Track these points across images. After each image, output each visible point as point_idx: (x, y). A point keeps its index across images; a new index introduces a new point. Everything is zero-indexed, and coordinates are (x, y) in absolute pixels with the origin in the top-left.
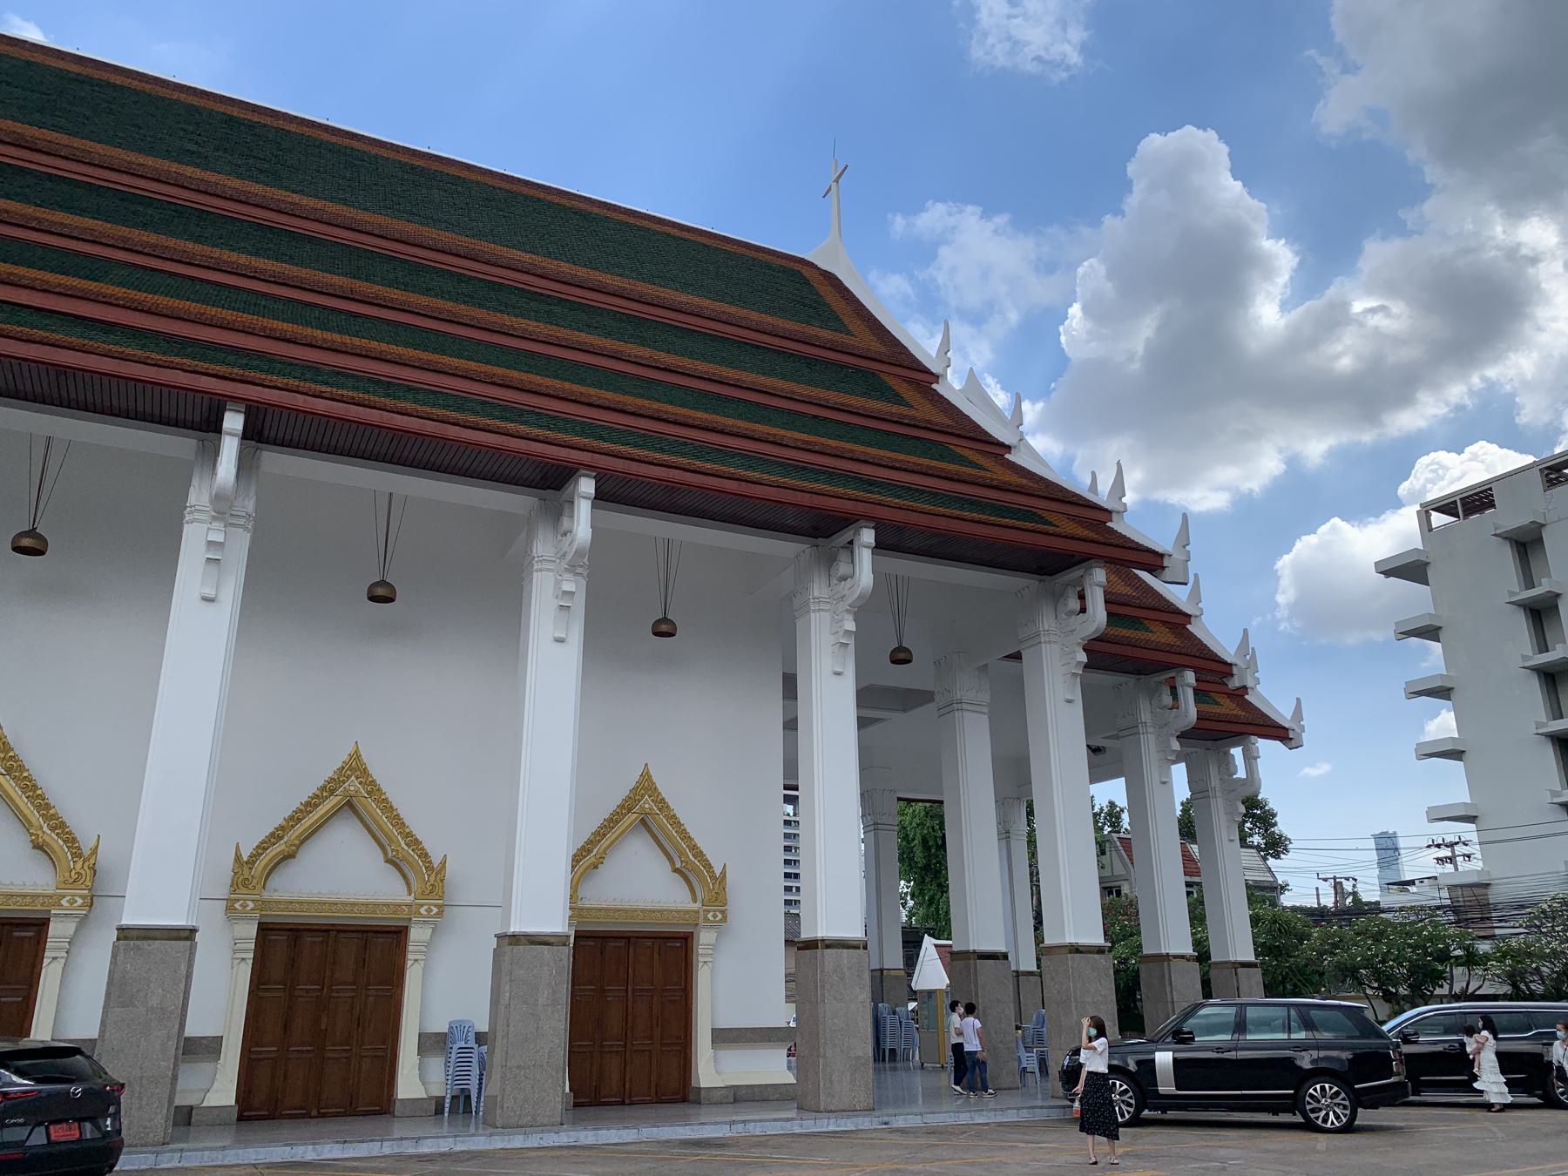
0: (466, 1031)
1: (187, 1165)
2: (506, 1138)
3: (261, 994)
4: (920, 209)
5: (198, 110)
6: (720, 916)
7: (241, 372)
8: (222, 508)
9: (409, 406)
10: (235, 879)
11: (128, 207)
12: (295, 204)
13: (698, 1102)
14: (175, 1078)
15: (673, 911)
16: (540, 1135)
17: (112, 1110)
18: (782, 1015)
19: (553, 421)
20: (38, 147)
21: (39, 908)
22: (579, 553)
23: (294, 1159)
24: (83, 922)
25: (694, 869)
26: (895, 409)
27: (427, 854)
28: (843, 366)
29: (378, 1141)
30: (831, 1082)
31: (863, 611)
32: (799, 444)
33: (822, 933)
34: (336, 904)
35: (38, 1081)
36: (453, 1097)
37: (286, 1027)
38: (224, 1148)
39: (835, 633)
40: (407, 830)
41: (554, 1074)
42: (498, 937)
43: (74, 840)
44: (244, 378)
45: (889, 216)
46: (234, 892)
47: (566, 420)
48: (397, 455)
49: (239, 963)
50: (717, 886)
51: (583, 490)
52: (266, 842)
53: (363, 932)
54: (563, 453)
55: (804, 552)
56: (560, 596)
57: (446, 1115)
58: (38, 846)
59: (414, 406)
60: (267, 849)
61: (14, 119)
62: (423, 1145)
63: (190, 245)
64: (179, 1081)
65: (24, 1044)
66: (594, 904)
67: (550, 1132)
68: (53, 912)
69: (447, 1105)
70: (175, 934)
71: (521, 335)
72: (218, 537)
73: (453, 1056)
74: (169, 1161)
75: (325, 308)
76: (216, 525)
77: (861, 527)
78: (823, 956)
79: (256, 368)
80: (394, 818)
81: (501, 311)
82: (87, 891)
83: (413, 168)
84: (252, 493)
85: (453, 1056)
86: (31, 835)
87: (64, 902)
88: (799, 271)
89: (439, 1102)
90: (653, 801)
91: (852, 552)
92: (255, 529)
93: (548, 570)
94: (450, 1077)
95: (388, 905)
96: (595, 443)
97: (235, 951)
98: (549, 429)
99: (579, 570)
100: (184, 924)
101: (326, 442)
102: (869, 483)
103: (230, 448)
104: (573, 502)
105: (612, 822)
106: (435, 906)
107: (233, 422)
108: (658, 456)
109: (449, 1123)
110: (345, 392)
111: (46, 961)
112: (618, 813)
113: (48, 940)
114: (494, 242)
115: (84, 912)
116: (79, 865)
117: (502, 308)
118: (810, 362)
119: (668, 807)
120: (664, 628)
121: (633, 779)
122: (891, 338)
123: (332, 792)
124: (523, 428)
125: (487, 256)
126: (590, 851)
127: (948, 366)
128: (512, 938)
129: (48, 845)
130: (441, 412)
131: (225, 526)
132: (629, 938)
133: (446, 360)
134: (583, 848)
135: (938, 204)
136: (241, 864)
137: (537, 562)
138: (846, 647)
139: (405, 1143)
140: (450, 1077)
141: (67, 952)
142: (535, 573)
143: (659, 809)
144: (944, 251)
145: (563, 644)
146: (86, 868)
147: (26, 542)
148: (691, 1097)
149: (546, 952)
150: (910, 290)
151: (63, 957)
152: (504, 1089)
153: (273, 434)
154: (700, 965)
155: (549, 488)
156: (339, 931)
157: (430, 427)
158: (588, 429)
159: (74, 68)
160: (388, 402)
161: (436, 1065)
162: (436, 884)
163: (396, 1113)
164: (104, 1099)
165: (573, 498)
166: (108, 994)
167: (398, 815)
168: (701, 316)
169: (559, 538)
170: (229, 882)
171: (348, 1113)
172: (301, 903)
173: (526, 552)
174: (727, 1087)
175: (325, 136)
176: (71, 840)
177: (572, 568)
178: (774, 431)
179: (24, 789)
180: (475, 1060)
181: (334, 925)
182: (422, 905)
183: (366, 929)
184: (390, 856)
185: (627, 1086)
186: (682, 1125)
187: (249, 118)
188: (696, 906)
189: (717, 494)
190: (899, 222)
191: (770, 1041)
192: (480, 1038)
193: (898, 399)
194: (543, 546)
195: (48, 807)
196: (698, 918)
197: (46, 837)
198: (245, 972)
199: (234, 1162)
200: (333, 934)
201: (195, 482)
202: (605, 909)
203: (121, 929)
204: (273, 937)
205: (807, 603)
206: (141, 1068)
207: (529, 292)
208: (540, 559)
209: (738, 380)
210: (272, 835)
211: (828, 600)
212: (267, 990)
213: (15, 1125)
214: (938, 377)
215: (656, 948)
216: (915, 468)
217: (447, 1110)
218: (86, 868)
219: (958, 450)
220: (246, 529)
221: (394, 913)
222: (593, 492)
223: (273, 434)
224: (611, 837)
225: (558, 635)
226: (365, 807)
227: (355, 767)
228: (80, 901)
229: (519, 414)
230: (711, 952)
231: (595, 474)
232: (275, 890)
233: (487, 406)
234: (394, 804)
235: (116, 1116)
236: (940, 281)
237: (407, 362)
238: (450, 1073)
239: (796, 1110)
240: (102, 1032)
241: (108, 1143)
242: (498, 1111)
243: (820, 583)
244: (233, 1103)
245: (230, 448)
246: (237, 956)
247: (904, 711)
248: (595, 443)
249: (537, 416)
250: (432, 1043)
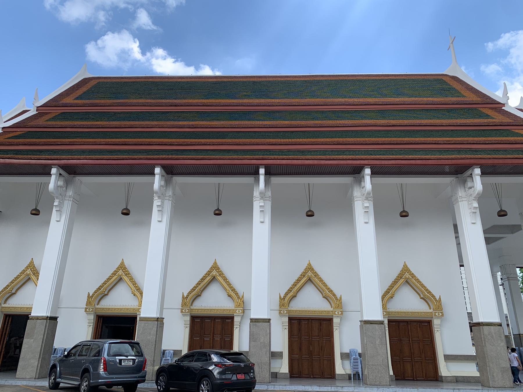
0: (355, 352)
1: (276, 389)
2: (371, 388)
3: (292, 339)
4: (499, 37)
5: (245, 82)
6: (441, 314)
7: (262, 157)
8: (263, 196)
9: (309, 157)
10: (280, 304)
11: (232, 115)
12: (273, 102)
13: (442, 381)
14: (270, 364)
15: (423, 312)
16: (383, 389)
17: (252, 371)
18: (472, 351)
19: (355, 152)
20: (208, 105)
21: (231, 313)
22: (368, 194)
23: (305, 390)
24: (242, 317)
25: (428, 297)
26: (486, 121)
27: (335, 295)
28: (462, 109)
29: (330, 386)
30: (493, 376)
31: (481, 198)
32: (445, 142)
33: (481, 320)
34: (310, 311)
35: (233, 362)
36: (354, 374)
37: (300, 349)
38: (285, 385)
39: (470, 209)
40: (328, 287)
41: (385, 368)
42: (361, 321)
43: (237, 294)
44: (263, 158)
45: (485, 44)
46: (280, 308)
47: (358, 151)
48: (308, 172)
49: (285, 329)
50: (438, 303)
51: (367, 173)
52: (96, 291)
53: (319, 320)
54: (358, 162)
55: (453, 180)
56: (364, 208)
57: (352, 380)
58: (229, 296)
59: (311, 157)
60: (191, 293)
61: (202, 99)
62: (344, 389)
63: (247, 122)
64: (271, 364)
65: (232, 351)
66: (393, 310)
67: (386, 388)
68: (235, 314)
69: (352, 377)
70: (265, 320)
71: (343, 126)
72: (262, 204)
73: (352, 360)
74: (271, 388)
75: (284, 131)
76: (261, 201)
77: (474, 168)
78: (483, 328)
79: (267, 155)
80: (323, 283)
81: (336, 120)
82: (242, 308)
83: (306, 81)
84: (270, 190)
85: (352, 360)
86: (227, 292)
87: (237, 311)
88: (441, 79)
89: (350, 376)
90: (409, 274)
91: (472, 178)
92: (272, 200)
93: (359, 200)
94: (352, 368)
95: (325, 311)
96: (369, 157)
97: (283, 326)
98: (353, 155)
99: (369, 199)
100: (267, 318)
101: (288, 172)
102: (476, 151)
103: (262, 178)
104: (364, 177)
105: (395, 282)
107: (262, 171)
108: (391, 156)
109: (353, 382)
110: (290, 157)
111: (235, 328)
112: (397, 279)
114: (332, 98)
115: (242, 314)
116: (239, 301)
117: (337, 118)
118: (449, 110)
119: (415, 276)
120: (404, 214)
121: (401, 267)
122: (482, 94)
123: (304, 276)
124: (345, 157)
125: (330, 103)
126: (389, 292)
127: (508, 99)
128: (365, 322)
129: (231, 295)
130: (319, 157)
131: (264, 201)
132: (408, 322)
133: (319, 140)
134: (386, 291)
135: (506, 34)
136: (282, 299)
137: (355, 198)
138: (476, 213)
139: (338, 388)
140: (352, 368)
141: (239, 326)
142: (355, 202)
143: (412, 277)
144: (512, 51)
145: (368, 224)
146: (241, 301)
147: (217, 212)
148: (439, 379)
149: (377, 327)
150: (500, 69)
151: (238, 327)
152: (369, 372)
153: (273, 172)
154: (436, 331)
155: (356, 174)
156: (312, 320)
157: (316, 162)
158: (367, 152)
159: (215, 80)
160: (303, 157)
161: (347, 363)
162: (339, 304)
163: (336, 378)
164: (249, 368)
165: (364, 176)
166: (250, 338)
167: (324, 282)
168: (405, 104)
169: (361, 189)
170: (279, 305)
171: (322, 377)
172: (300, 311)
173: (352, 196)
174: (453, 376)
175: (279, 79)
176: (237, 294)
177: (367, 199)
178: (435, 139)
179: (224, 280)
180: (359, 362)
181: (310, 318)
182: (336, 311)
183: (319, 319)
184: (324, 295)
185: (414, 374)
186: (434, 389)
187: (259, 80)
188: (431, 311)
189: (415, 166)
190: (490, 46)
191: (468, 360)
192: (360, 355)
193: (488, 116)
194: (357, 193)
195: (230, 284)
196: (433, 315)
197: (231, 293)
198: (287, 332)
199: (288, 390)
200: (310, 321)
201: (255, 189)
202: (398, 312)
203: (251, 319)
204: (293, 322)
205: (457, 199)
206: (261, 360)
207: (345, 111)
208: (356, 197)
209: (421, 123)
210: (289, 290)
211: (465, 197)
212: (294, 338)
213: (228, 374)
214: (504, 104)
215: (418, 325)
216: (496, 142)
217: (352, 378)
218: (241, 301)
219: (516, 131)
220: (269, 201)
221: (321, 313)
222: (370, 173)
223: (273, 172)
224: (395, 287)
225: (365, 221)
226: (314, 280)
227: (310, 268)
228: (241, 311)
229: (343, 152)
230: (439, 327)
231: (370, 167)
232: (292, 307)
233: (333, 151)
234: (323, 279)
235: (253, 373)
236: (513, 62)
237: (308, 143)
238: (352, 366)
239: (481, 386)
240: (250, 349)
241: (252, 381)
242: (368, 379)
243: (461, 190)
244: (288, 372)
245: (262, 178)
246: (284, 327)
247: (512, 233)
248: (369, 157)
249: (349, 151)
250: (345, 356)
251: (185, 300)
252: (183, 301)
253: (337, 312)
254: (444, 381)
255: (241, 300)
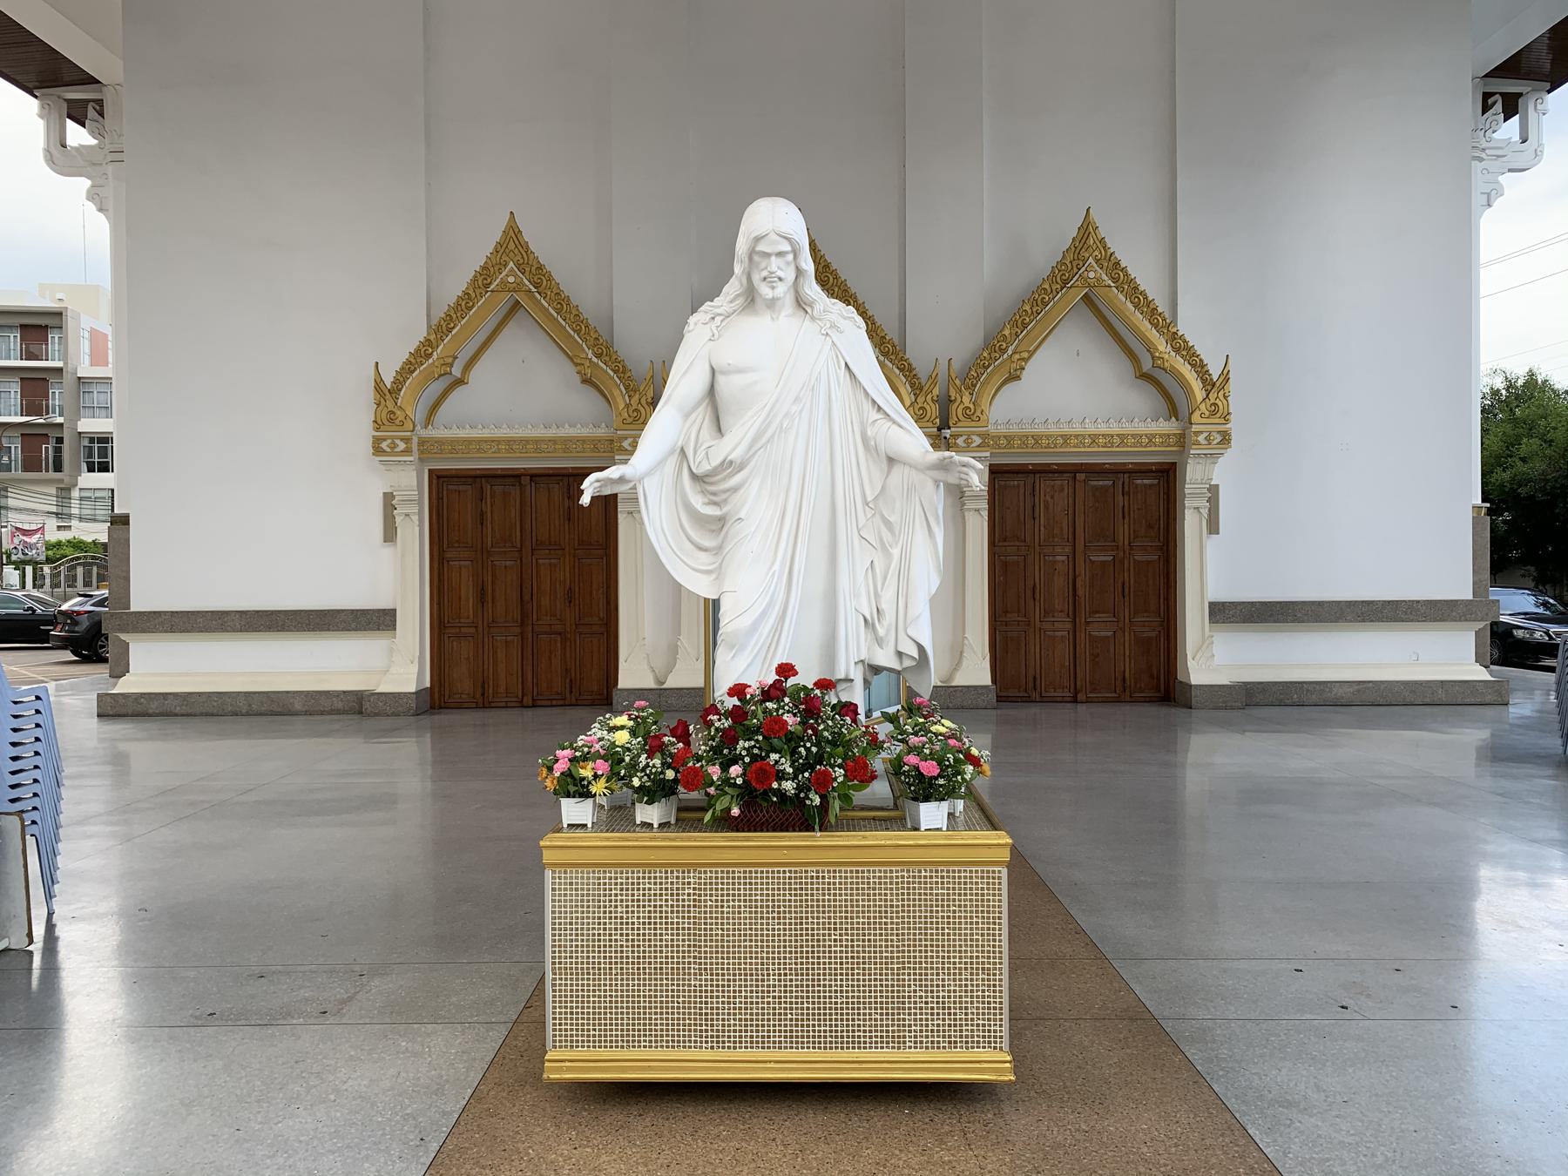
106: (402, 440)
113: (1186, 486)
136: (385, 394)
251: (390, 404)
252: (378, 405)
253: (389, 441)
254: (1193, 707)
255: (929, 397)
